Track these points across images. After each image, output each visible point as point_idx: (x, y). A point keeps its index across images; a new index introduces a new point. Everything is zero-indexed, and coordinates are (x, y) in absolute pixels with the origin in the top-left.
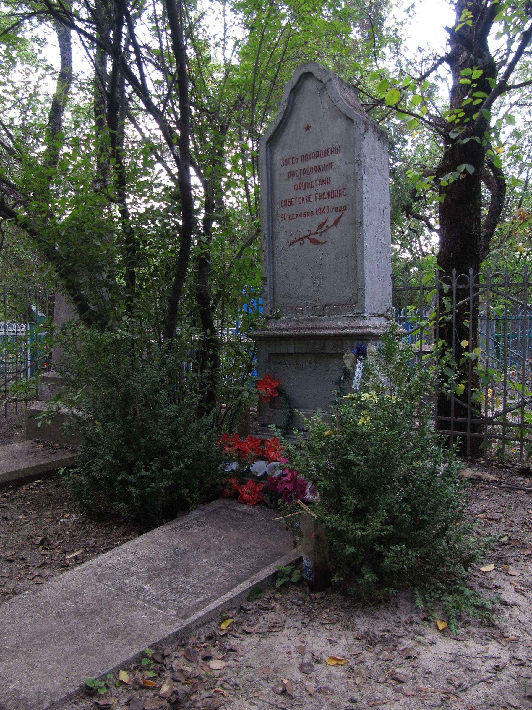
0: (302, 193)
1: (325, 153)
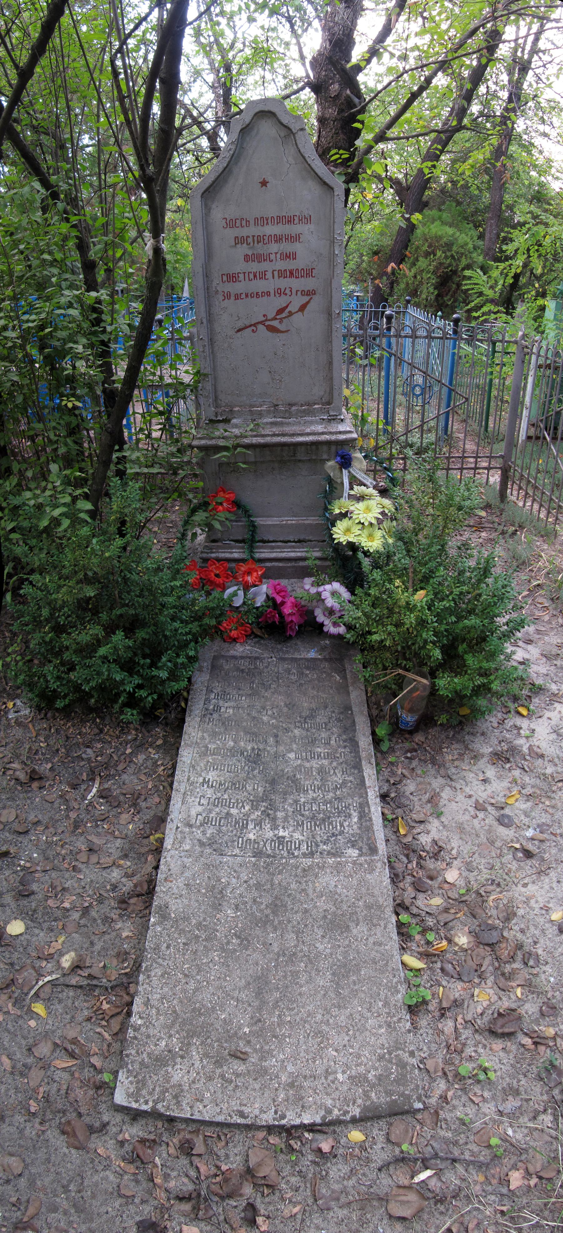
0: (254, 267)
1: (290, 220)
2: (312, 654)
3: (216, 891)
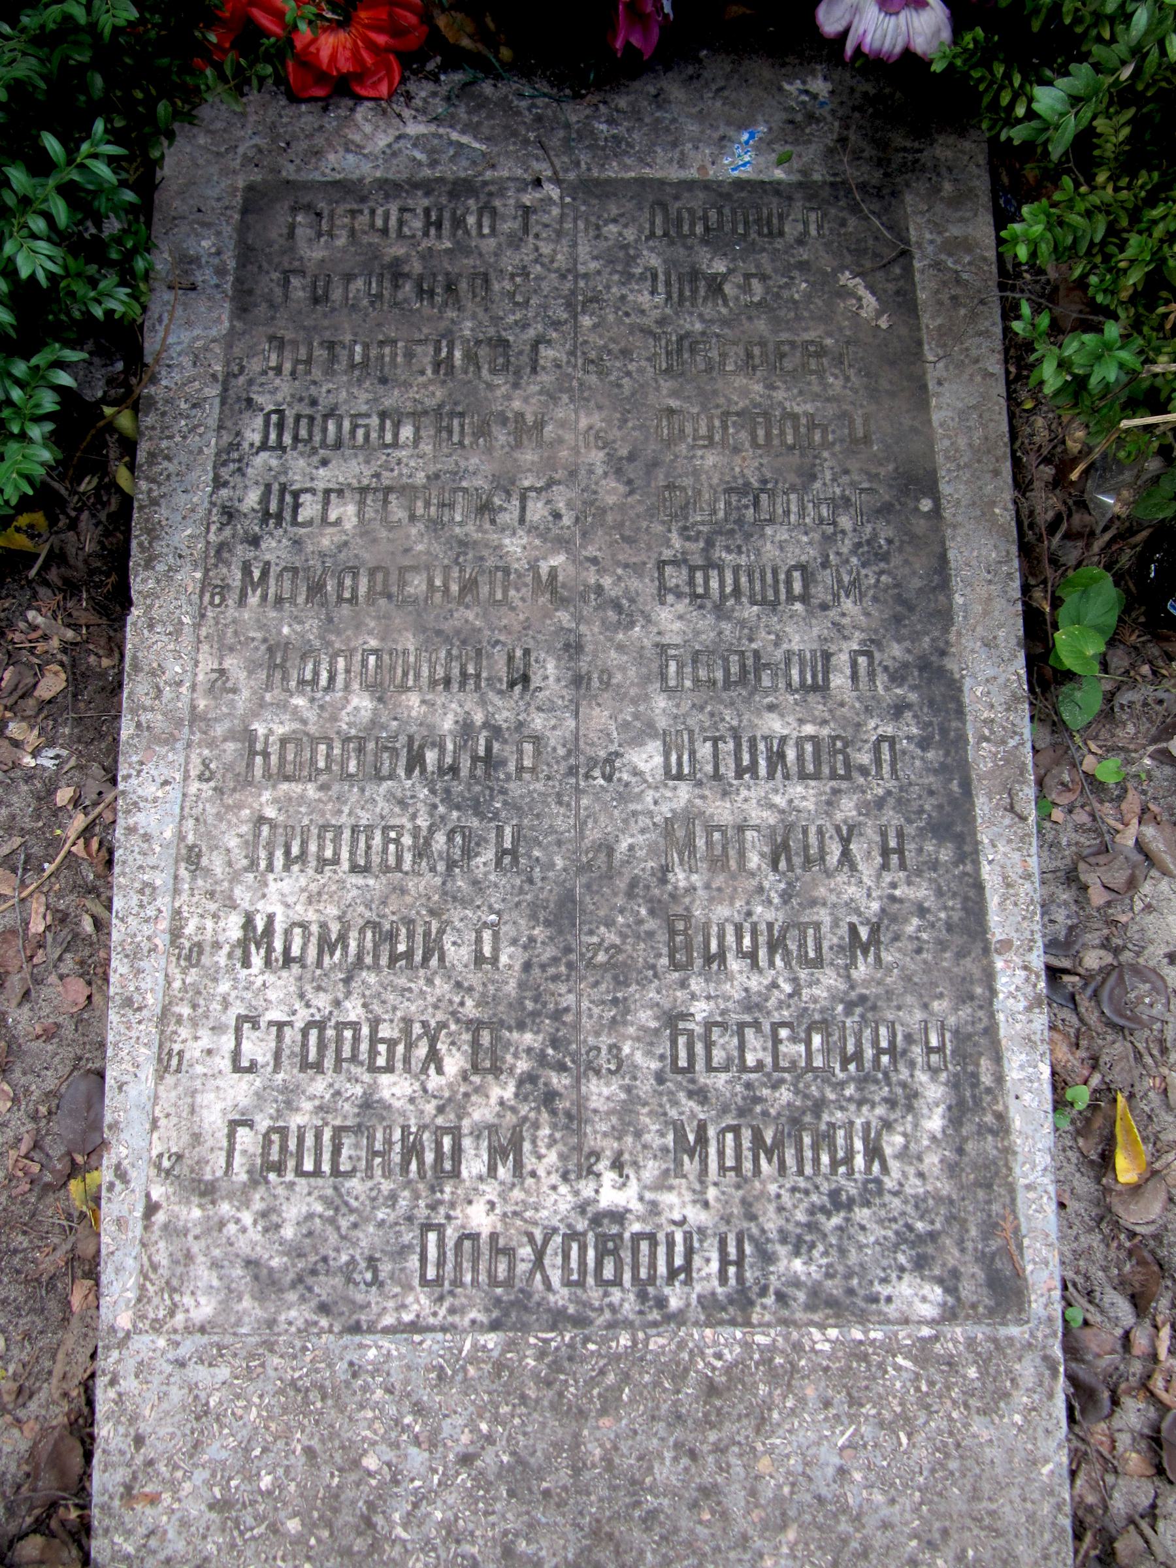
2: (742, 161)
3: (346, 1517)
